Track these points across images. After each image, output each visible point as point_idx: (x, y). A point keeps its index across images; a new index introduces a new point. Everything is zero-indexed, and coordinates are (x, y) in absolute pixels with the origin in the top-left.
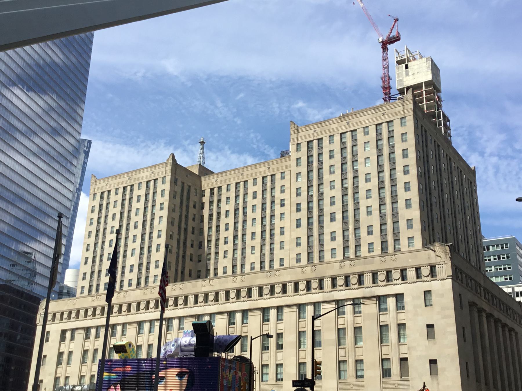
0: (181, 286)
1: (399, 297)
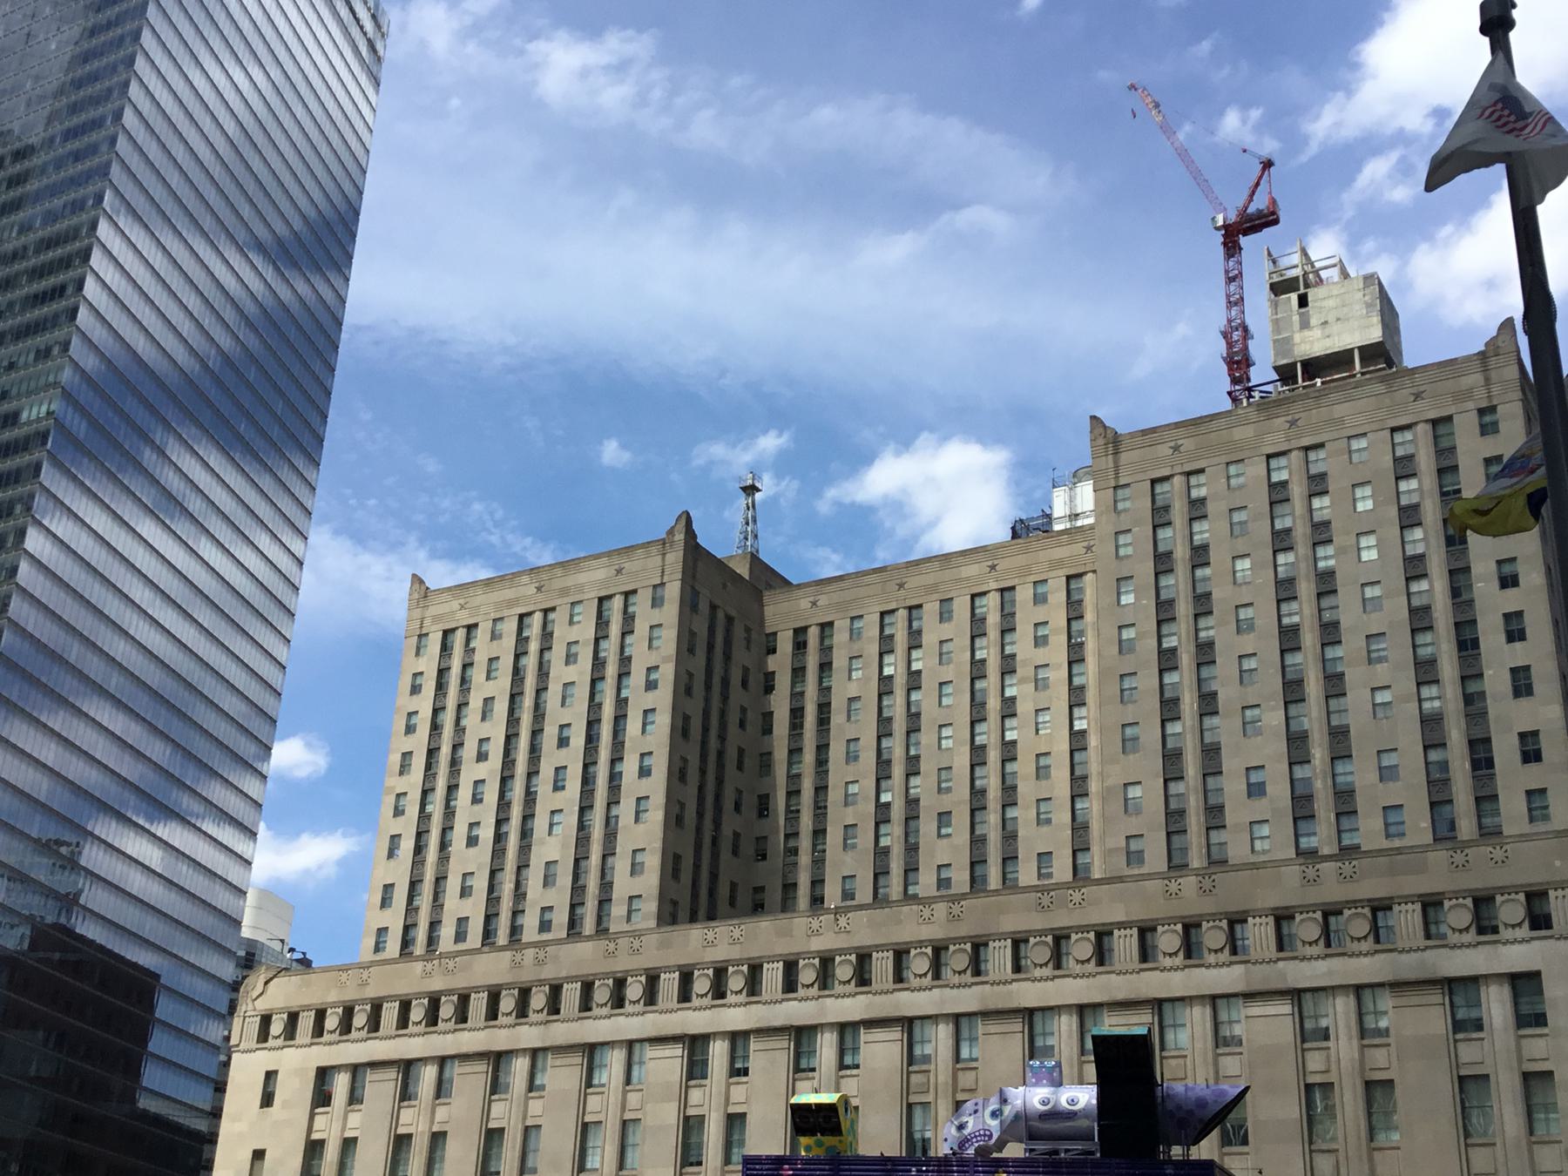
0: (737, 933)
1: (1525, 984)
